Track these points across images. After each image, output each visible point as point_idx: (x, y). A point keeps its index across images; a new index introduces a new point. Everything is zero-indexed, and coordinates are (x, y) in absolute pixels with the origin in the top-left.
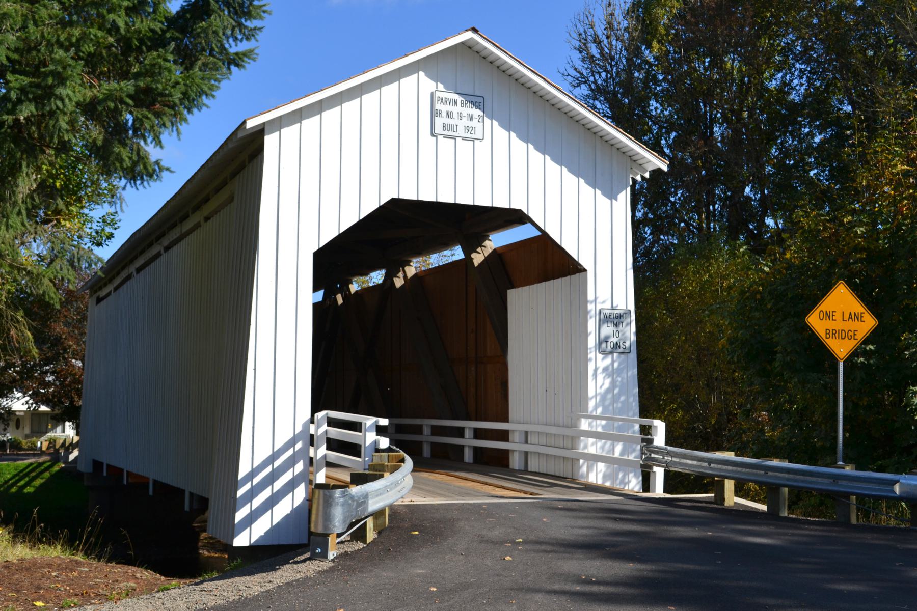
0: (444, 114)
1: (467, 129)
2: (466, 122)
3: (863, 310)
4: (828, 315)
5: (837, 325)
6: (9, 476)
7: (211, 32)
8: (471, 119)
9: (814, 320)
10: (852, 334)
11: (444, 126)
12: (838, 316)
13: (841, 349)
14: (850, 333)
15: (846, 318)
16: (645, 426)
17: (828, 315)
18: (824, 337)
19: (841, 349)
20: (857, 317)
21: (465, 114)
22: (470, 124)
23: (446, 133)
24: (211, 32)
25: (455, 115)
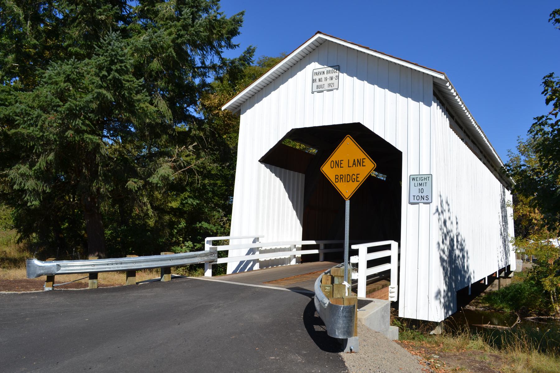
0: (317, 80)
1: (329, 85)
2: (329, 81)
3: (364, 156)
4: (338, 164)
5: (345, 171)
6: (185, 284)
7: (39, 127)
8: (332, 79)
9: (327, 170)
10: (355, 177)
11: (317, 87)
12: (345, 164)
13: (347, 190)
14: (354, 177)
15: (351, 165)
16: (390, 277)
17: (338, 164)
18: (334, 181)
19: (347, 190)
20: (359, 163)
21: (328, 77)
22: (331, 82)
23: (319, 90)
24: (39, 127)
25: (323, 79)
